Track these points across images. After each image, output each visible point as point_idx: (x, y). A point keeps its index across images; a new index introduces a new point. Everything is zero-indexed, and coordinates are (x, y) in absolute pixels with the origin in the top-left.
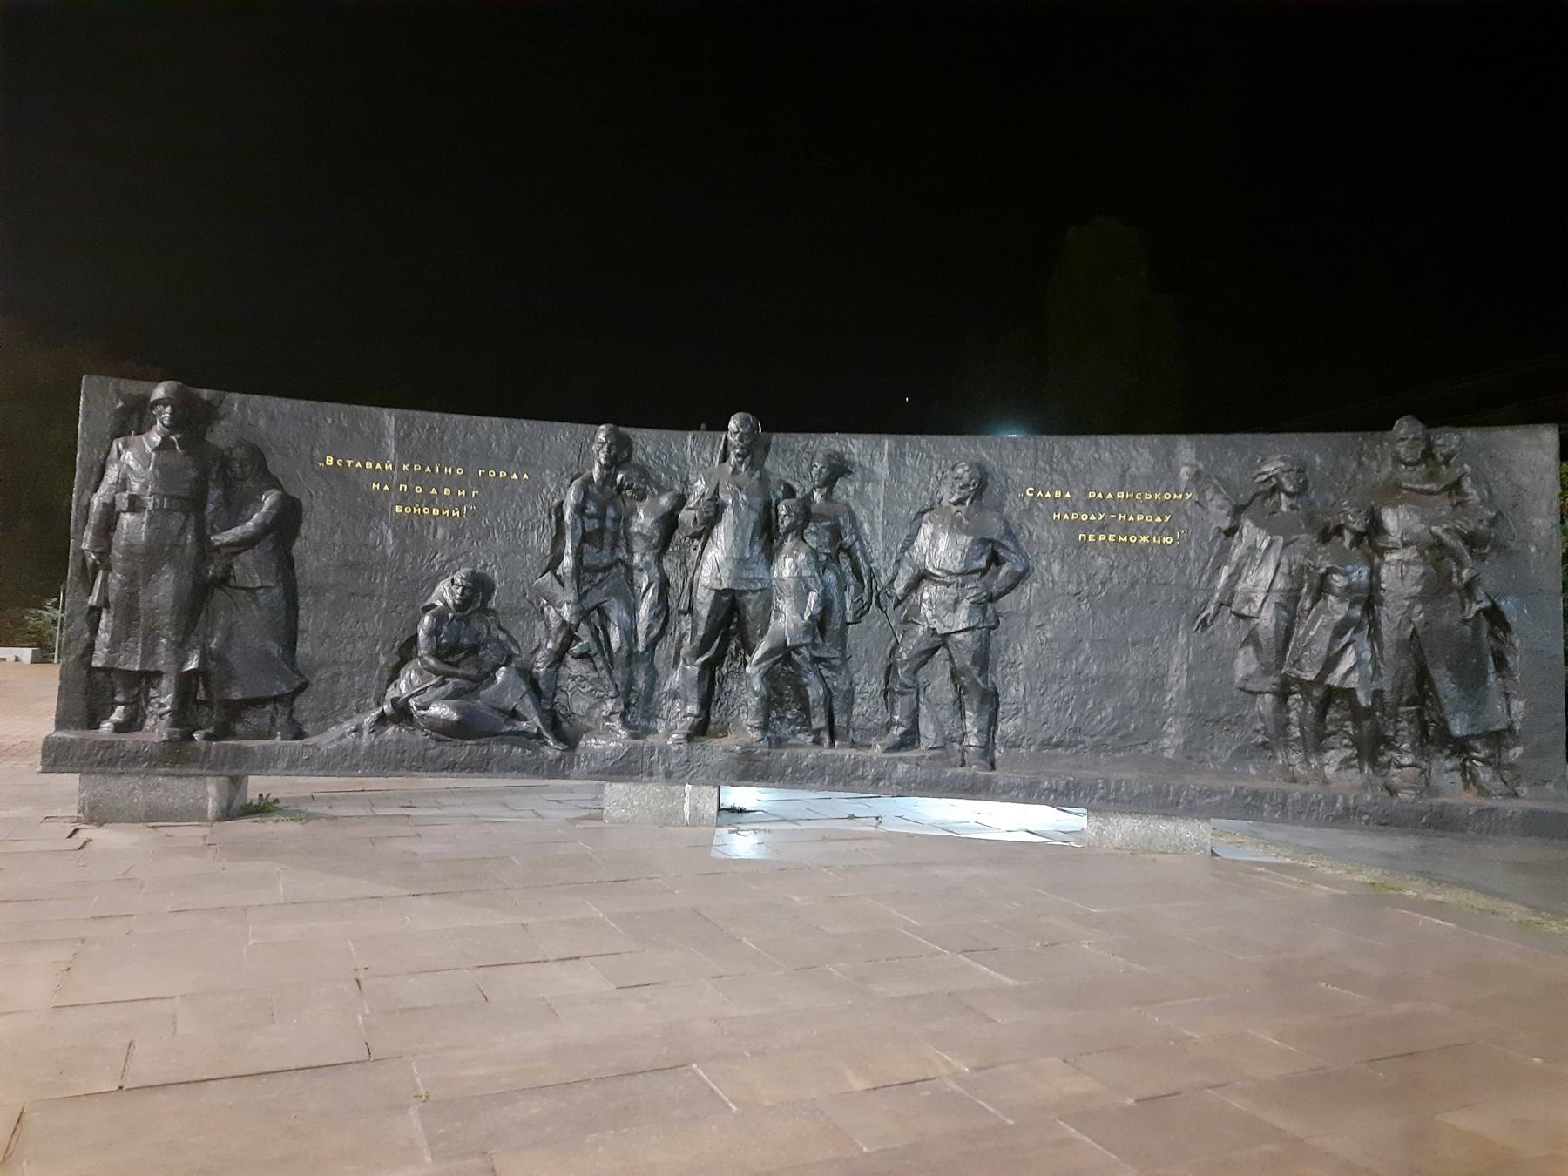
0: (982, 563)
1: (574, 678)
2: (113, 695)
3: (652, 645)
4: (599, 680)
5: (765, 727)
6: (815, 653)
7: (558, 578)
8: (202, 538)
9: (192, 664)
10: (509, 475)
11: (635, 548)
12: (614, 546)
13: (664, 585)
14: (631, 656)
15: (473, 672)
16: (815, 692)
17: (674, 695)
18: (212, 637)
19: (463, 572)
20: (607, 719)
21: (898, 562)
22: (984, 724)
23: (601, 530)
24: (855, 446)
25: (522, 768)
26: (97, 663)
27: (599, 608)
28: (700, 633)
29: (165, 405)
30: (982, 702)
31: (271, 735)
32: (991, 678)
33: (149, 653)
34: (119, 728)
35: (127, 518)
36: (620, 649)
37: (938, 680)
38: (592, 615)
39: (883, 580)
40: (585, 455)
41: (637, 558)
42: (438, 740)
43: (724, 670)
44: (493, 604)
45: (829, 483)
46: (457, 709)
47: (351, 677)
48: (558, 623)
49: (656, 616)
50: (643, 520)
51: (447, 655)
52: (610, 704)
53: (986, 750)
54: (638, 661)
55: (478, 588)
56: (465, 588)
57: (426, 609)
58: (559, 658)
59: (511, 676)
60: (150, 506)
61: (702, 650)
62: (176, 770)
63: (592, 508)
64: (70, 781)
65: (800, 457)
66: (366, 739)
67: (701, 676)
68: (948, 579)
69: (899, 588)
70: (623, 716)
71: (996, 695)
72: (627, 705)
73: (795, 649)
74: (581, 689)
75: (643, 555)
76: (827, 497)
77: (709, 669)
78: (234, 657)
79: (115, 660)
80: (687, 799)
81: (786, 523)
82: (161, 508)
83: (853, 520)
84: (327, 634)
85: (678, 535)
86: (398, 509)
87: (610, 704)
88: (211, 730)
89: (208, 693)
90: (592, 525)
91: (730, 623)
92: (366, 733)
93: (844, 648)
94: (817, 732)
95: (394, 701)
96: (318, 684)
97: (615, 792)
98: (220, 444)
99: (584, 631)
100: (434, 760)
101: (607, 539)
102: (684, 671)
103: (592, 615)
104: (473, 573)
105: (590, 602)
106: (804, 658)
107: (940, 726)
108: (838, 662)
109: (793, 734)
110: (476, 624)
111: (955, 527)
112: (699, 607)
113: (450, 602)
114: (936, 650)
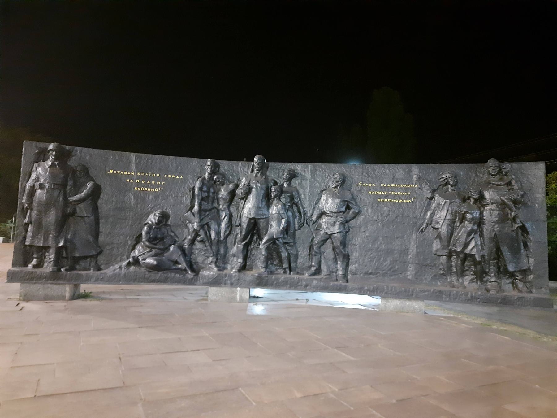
0: (344, 209)
1: (198, 249)
3: (226, 237)
5: (266, 267)
6: (285, 241)
7: (193, 214)
8: (65, 199)
9: (61, 244)
12: (213, 202)
13: (231, 216)
14: (219, 241)
15: (162, 247)
16: (284, 255)
17: (234, 255)
22: (344, 266)
24: (299, 167)
25: (178, 282)
26: (27, 243)
27: (207, 224)
28: (243, 233)
30: (344, 258)
32: (347, 250)
33: (46, 239)
35: (39, 192)
36: (214, 239)
39: (309, 215)
40: (203, 170)
41: (221, 206)
42: (149, 272)
43: (252, 247)
44: (169, 223)
45: (289, 180)
46: (156, 260)
47: (118, 248)
48: (193, 229)
49: (228, 228)
50: (223, 193)
51: (152, 241)
53: (345, 276)
54: (221, 243)
55: (164, 217)
56: (159, 217)
58: (192, 242)
59: (175, 248)
60: (47, 187)
63: (205, 189)
64: (16, 286)
65: (279, 171)
66: (123, 271)
67: (243, 248)
68: (331, 215)
70: (216, 263)
71: (349, 256)
72: (217, 259)
73: (277, 239)
74: (201, 255)
76: (289, 185)
77: (246, 246)
79: (34, 242)
80: (238, 294)
85: (236, 199)
87: (211, 259)
88: (68, 267)
89: (67, 254)
91: (254, 230)
92: (123, 269)
93: (294, 239)
95: (133, 257)
97: (213, 290)
98: (73, 165)
99: (202, 233)
100: (147, 279)
102: (237, 247)
103: (205, 226)
107: (328, 267)
108: (292, 244)
109: (277, 269)
110: (163, 230)
111: (334, 196)
112: (243, 224)
114: (327, 240)
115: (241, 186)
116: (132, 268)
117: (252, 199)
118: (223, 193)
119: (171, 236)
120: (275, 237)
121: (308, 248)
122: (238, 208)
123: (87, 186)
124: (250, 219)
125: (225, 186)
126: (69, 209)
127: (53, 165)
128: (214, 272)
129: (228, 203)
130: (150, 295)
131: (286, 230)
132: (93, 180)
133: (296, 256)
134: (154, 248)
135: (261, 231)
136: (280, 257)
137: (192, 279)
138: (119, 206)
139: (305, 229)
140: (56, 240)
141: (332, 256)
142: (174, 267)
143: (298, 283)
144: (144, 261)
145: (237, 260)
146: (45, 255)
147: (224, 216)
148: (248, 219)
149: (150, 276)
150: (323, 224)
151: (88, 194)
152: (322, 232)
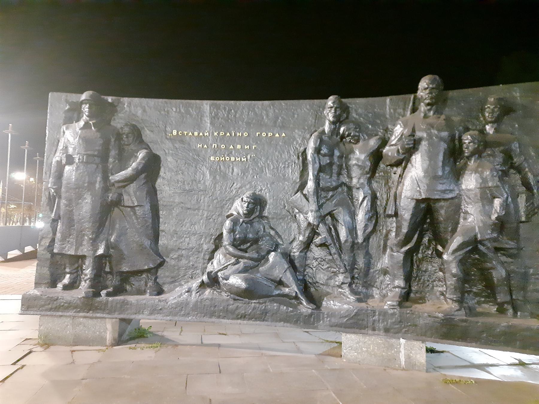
1: (316, 259)
2: (65, 269)
3: (367, 239)
4: (333, 261)
5: (461, 301)
7: (305, 196)
8: (105, 178)
9: (101, 251)
10: (274, 135)
11: (354, 175)
12: (339, 174)
13: (374, 198)
14: (354, 246)
15: (255, 256)
16: (499, 273)
17: (385, 272)
18: (112, 235)
19: (248, 193)
20: (340, 287)
23: (331, 164)
24: (517, 92)
26: (55, 251)
27: (331, 214)
28: (405, 230)
29: (86, 104)
31: (143, 293)
33: (79, 244)
34: (66, 288)
35: (67, 168)
36: (346, 241)
40: (319, 119)
41: (355, 181)
42: (235, 300)
43: (420, 256)
44: (266, 213)
46: (246, 280)
47: (188, 257)
48: (305, 224)
49: (370, 219)
50: (359, 156)
51: (240, 245)
52: (341, 278)
54: (358, 249)
55: (257, 203)
56: (249, 203)
57: (228, 217)
58: (307, 245)
59: (278, 258)
60: (77, 161)
62: (90, 314)
63: (324, 150)
64: (33, 319)
66: (194, 297)
70: (350, 285)
72: (353, 278)
73: (481, 242)
74: (322, 268)
75: (359, 179)
77: (409, 255)
78: (123, 246)
79: (64, 248)
80: (402, 350)
82: (82, 162)
84: (175, 232)
85: (382, 166)
86: (212, 158)
87: (341, 278)
88: (111, 290)
89: (111, 268)
90: (326, 160)
91: (425, 223)
92: (194, 293)
95: (209, 274)
96: (170, 261)
97: (350, 341)
98: (119, 126)
99: (322, 229)
100: (233, 312)
101: (335, 168)
102: (391, 256)
103: (327, 217)
104: (254, 194)
105: (324, 211)
106: (488, 248)
108: (515, 252)
110: (256, 225)
112: (401, 212)
113: (241, 212)
115: (394, 140)
116: (208, 292)
119: (271, 236)
122: (387, 183)
123: (137, 157)
124: (418, 202)
125: (361, 143)
126: (111, 195)
127: (87, 126)
128: (349, 303)
129: (367, 173)
130: (241, 334)
132: (148, 147)
134: (242, 257)
135: (442, 226)
137: (311, 315)
138: (187, 188)
140: (92, 245)
142: (277, 292)
144: (225, 282)
145: (393, 281)
146: (82, 268)
147: (361, 199)
148: (413, 204)
149: (237, 308)
151: (137, 168)
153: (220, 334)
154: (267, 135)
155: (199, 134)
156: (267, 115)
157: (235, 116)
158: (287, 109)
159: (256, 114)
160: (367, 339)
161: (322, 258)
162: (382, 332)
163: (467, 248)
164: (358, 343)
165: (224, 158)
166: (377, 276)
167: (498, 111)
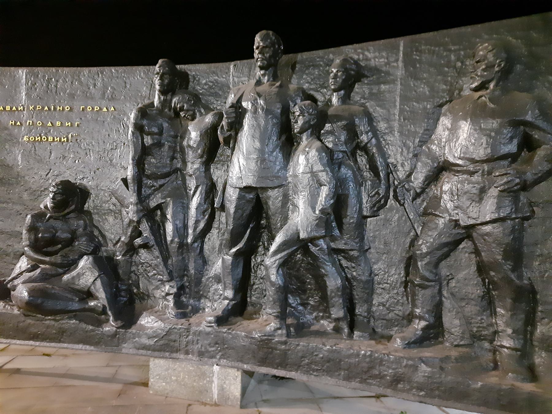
0: (512, 148)
5: (282, 316)
6: (333, 245)
14: (182, 245)
16: (333, 282)
17: (218, 279)
21: (415, 156)
22: (519, 324)
24: (370, 54)
25: (86, 340)
30: (516, 300)
32: (527, 274)
36: (172, 241)
37: (462, 272)
38: (152, 215)
39: (401, 174)
45: (347, 86)
50: (194, 135)
53: (524, 353)
61: (233, 242)
65: (321, 71)
67: (234, 264)
68: (471, 168)
69: (418, 179)
71: (534, 292)
73: (312, 240)
76: (346, 99)
81: (300, 122)
83: (370, 119)
93: (362, 239)
94: (337, 320)
103: (152, 215)
106: (321, 250)
107: (467, 321)
108: (355, 253)
109: (317, 319)
111: (477, 114)
114: (458, 242)
117: (246, 139)
118: (194, 135)
120: (303, 235)
121: (402, 266)
124: (247, 189)
125: (196, 120)
131: (335, 213)
133: (370, 287)
136: (321, 286)
139: (393, 212)
141: (475, 290)
143: (371, 368)
150: (446, 197)
152: (441, 222)
153: (44, 355)
154: (93, 109)
155: (11, 108)
156: (95, 85)
157: (56, 86)
158: (117, 77)
159: (81, 83)
160: (177, 365)
161: (147, 263)
162: (195, 356)
163: (288, 249)
164: (167, 370)
165: (39, 138)
166: (210, 285)
167: (342, 75)
